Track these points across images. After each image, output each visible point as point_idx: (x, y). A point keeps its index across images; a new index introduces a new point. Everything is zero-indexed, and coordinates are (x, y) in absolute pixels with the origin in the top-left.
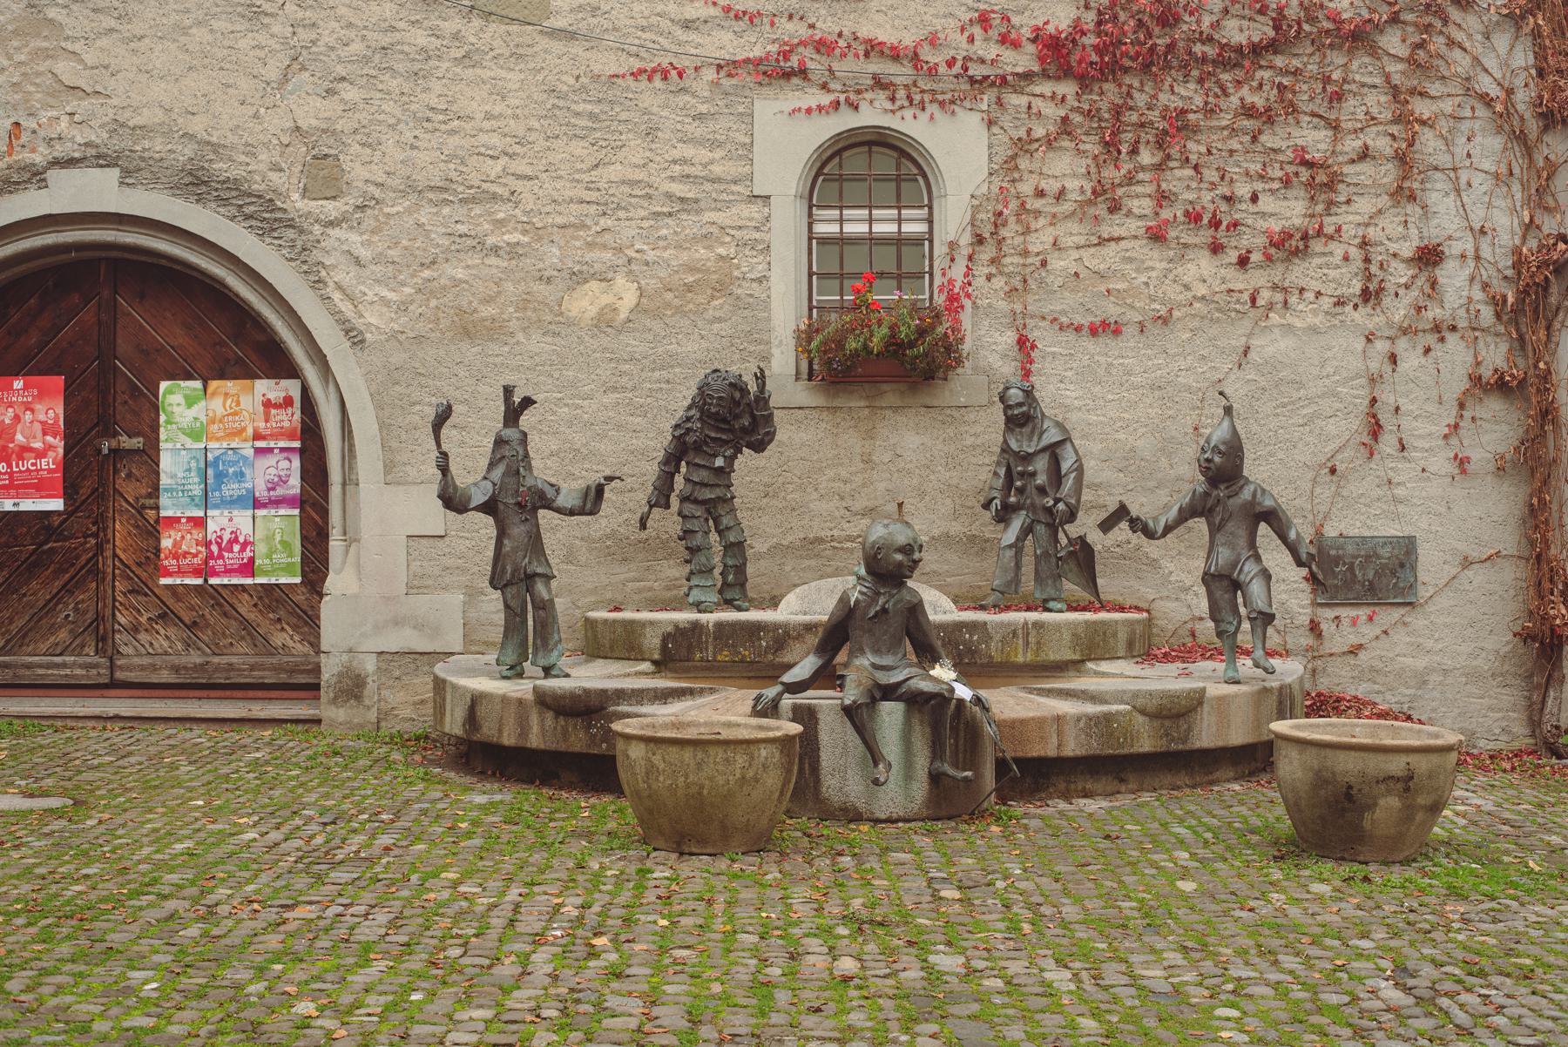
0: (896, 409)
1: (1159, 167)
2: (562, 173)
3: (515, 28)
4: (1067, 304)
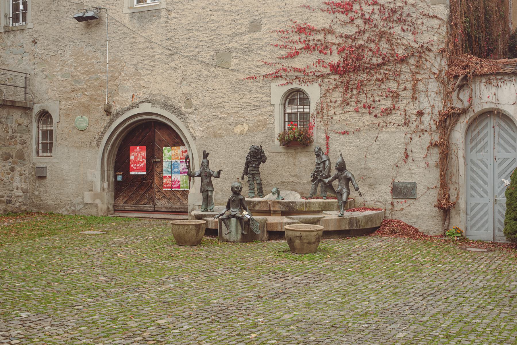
0: (300, 152)
1: (358, 94)
3: (224, 69)
4: (338, 127)
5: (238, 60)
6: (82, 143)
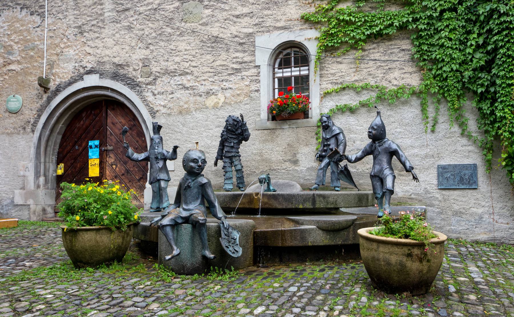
5: (210, 10)
6: (14, 129)
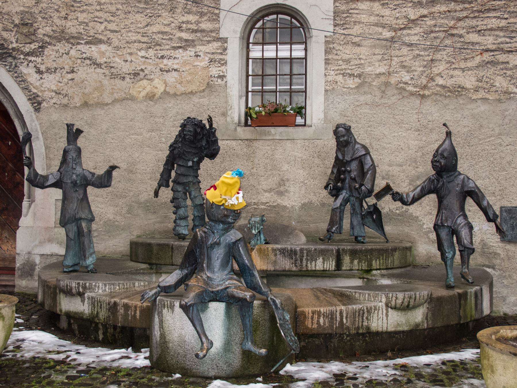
2: (131, 29)
